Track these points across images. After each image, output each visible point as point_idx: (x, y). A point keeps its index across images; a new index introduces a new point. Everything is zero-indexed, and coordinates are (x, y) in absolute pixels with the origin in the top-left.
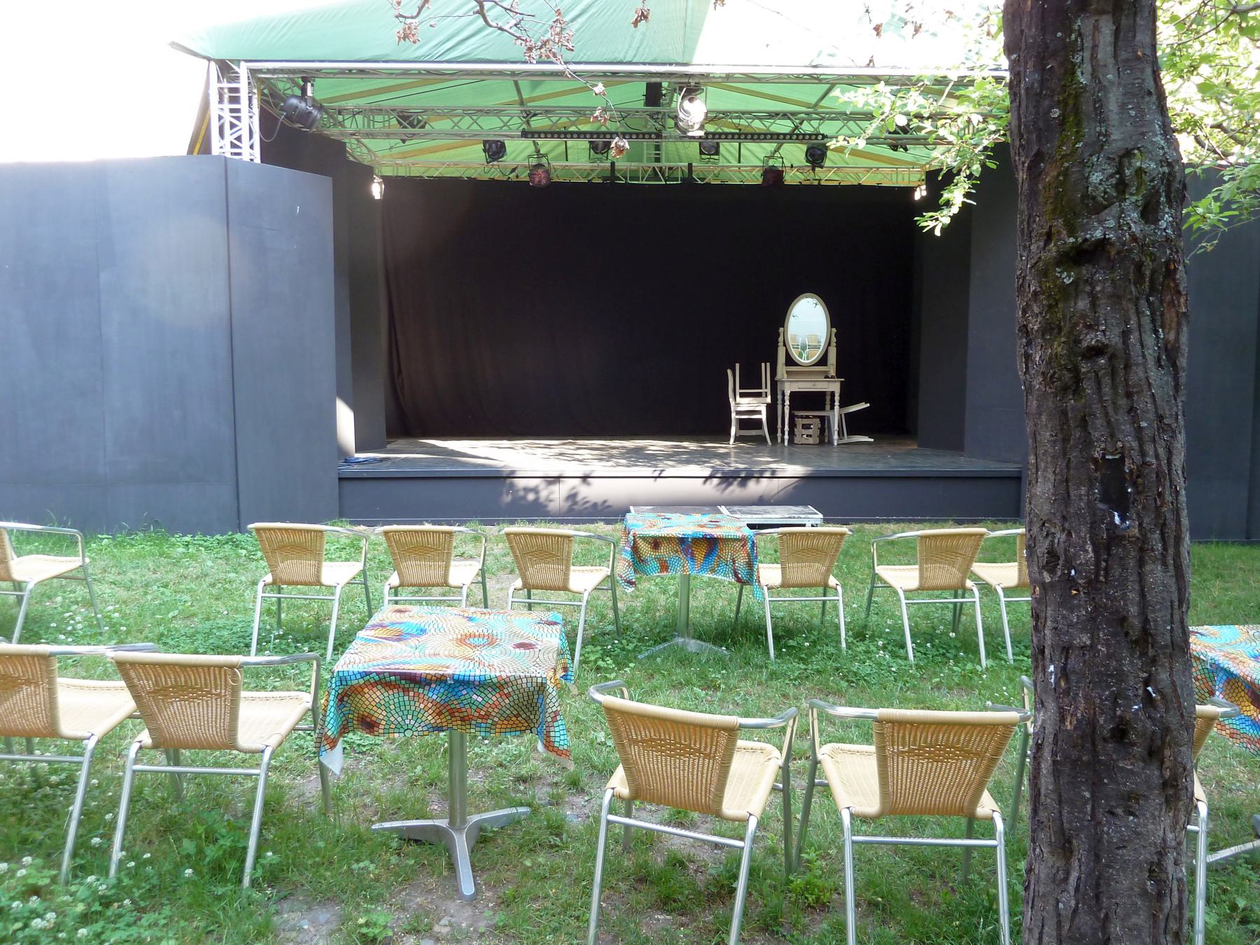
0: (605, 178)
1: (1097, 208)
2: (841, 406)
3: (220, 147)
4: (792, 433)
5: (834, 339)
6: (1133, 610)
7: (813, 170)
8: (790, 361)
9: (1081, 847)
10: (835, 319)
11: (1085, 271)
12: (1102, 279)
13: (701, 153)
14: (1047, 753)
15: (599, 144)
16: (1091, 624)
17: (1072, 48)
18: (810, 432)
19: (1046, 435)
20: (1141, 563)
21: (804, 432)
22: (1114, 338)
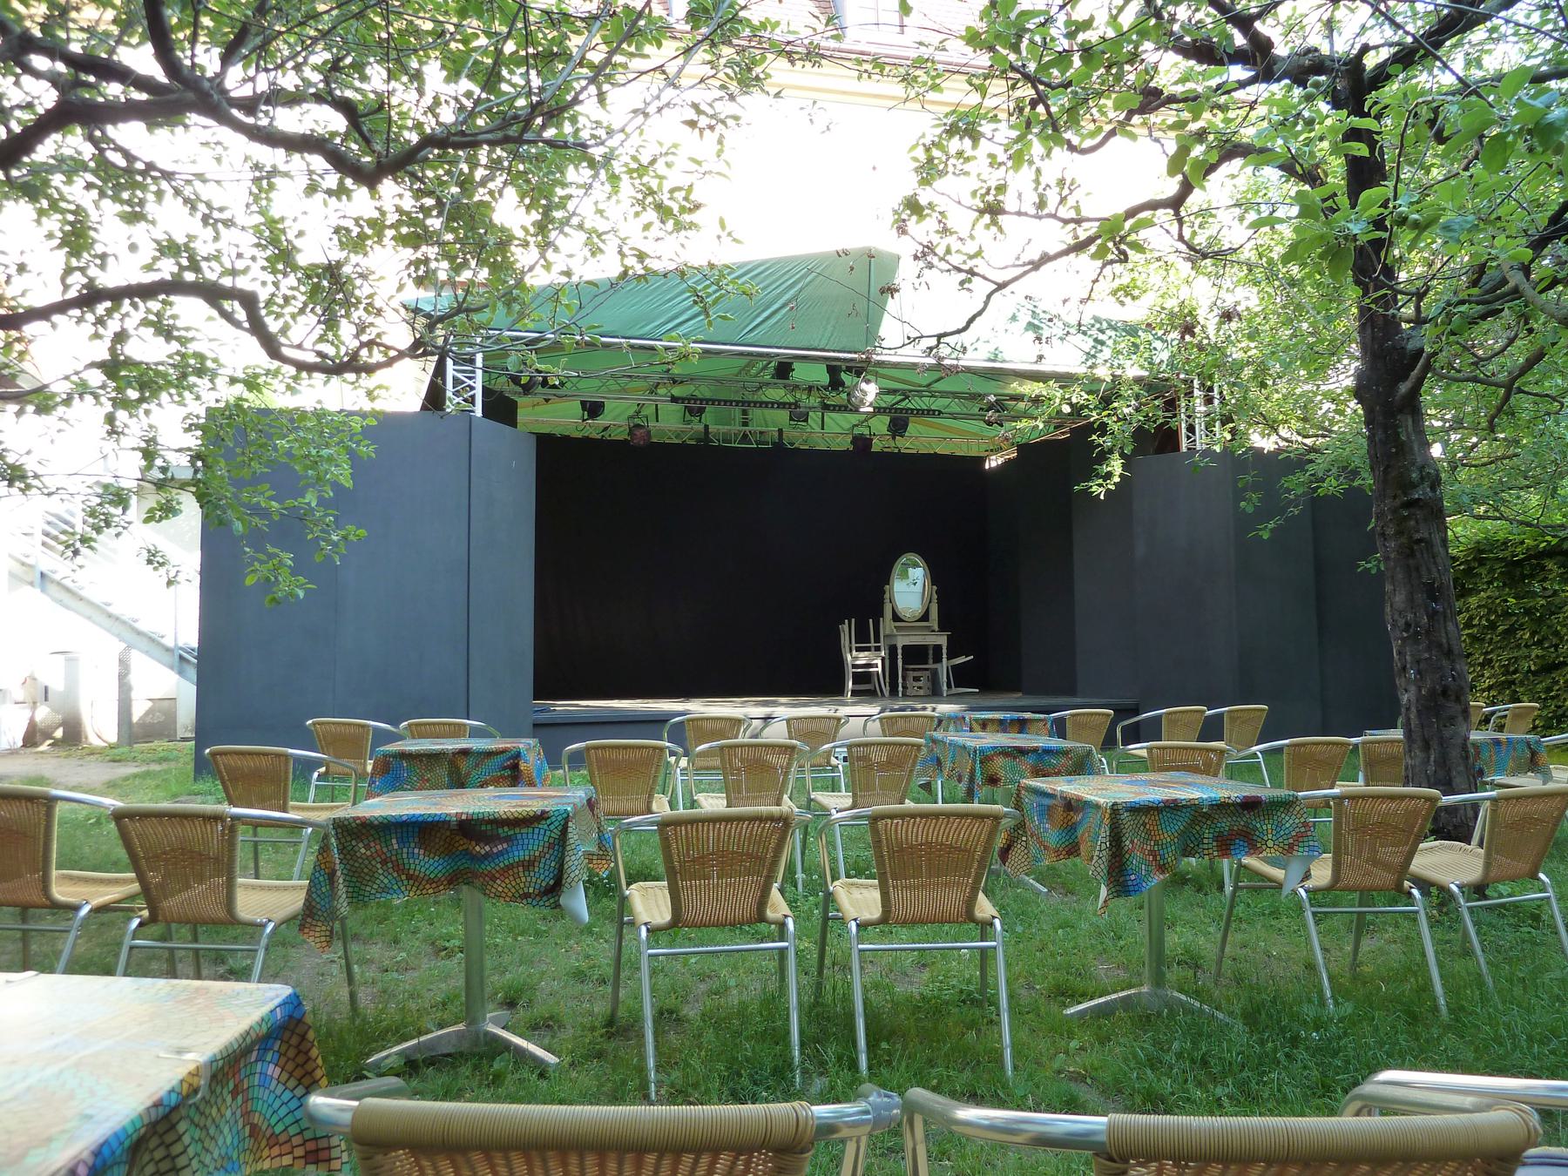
0: (699, 440)
1: (1414, 486)
2: (948, 659)
3: (452, 402)
4: (904, 687)
5: (935, 596)
6: (1444, 641)
7: (894, 438)
8: (896, 617)
9: (1434, 744)
10: (885, 578)
11: (1412, 510)
12: (1419, 514)
13: (791, 419)
14: (1413, 709)
15: (694, 407)
16: (1429, 649)
17: (1397, 426)
18: (920, 684)
19: (1400, 576)
20: (1445, 622)
21: (915, 684)
22: (1426, 535)
